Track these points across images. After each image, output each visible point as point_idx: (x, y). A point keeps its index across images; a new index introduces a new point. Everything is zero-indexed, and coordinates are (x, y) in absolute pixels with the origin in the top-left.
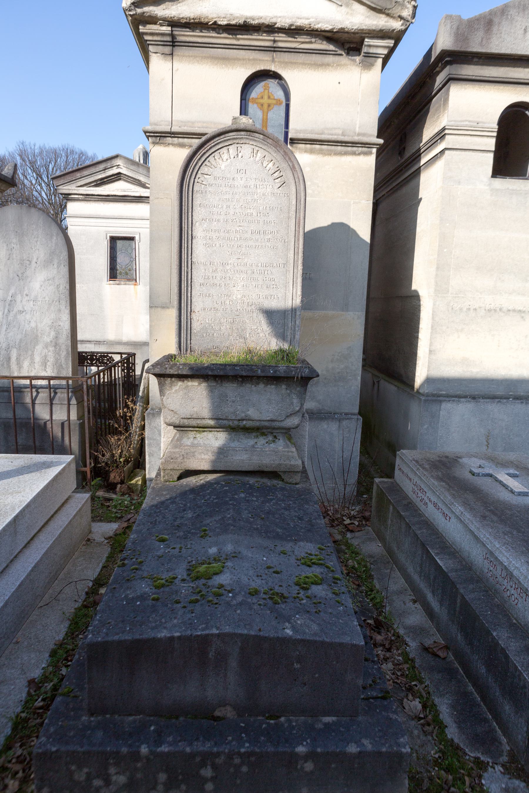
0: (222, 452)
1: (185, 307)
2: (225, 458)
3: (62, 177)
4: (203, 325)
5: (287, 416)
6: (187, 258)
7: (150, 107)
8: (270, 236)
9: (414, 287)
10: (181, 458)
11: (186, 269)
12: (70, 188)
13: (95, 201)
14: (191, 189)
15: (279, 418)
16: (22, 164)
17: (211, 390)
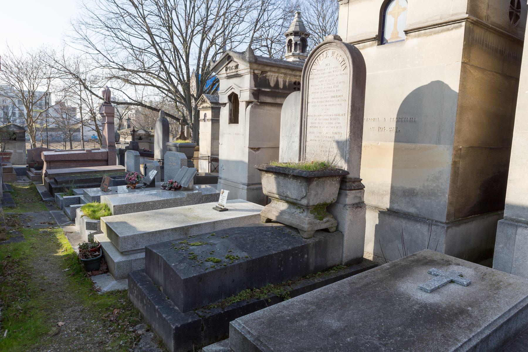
0: (282, 213)
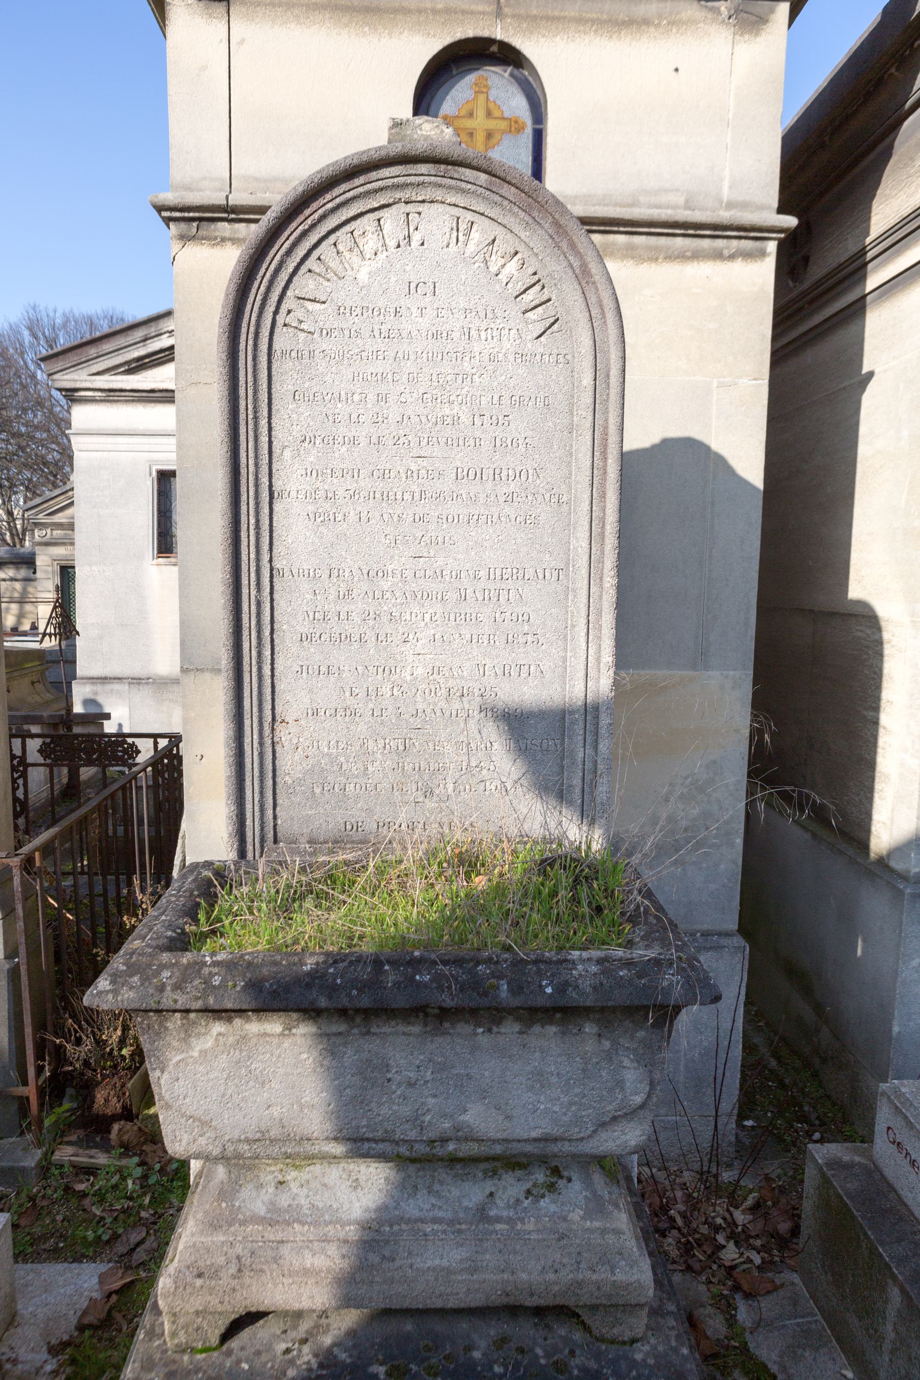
0: (377, 1241)
1: (255, 709)
2: (386, 1265)
3: (61, 357)
4: (311, 761)
5: (603, 1125)
6: (258, 560)
7: (171, 141)
8: (513, 486)
9: (855, 592)
10: (233, 1270)
11: (254, 593)
12: (76, 377)
13: (127, 401)
14: (263, 346)
15: (574, 1132)
16: (33, 344)
17: (331, 1047)
